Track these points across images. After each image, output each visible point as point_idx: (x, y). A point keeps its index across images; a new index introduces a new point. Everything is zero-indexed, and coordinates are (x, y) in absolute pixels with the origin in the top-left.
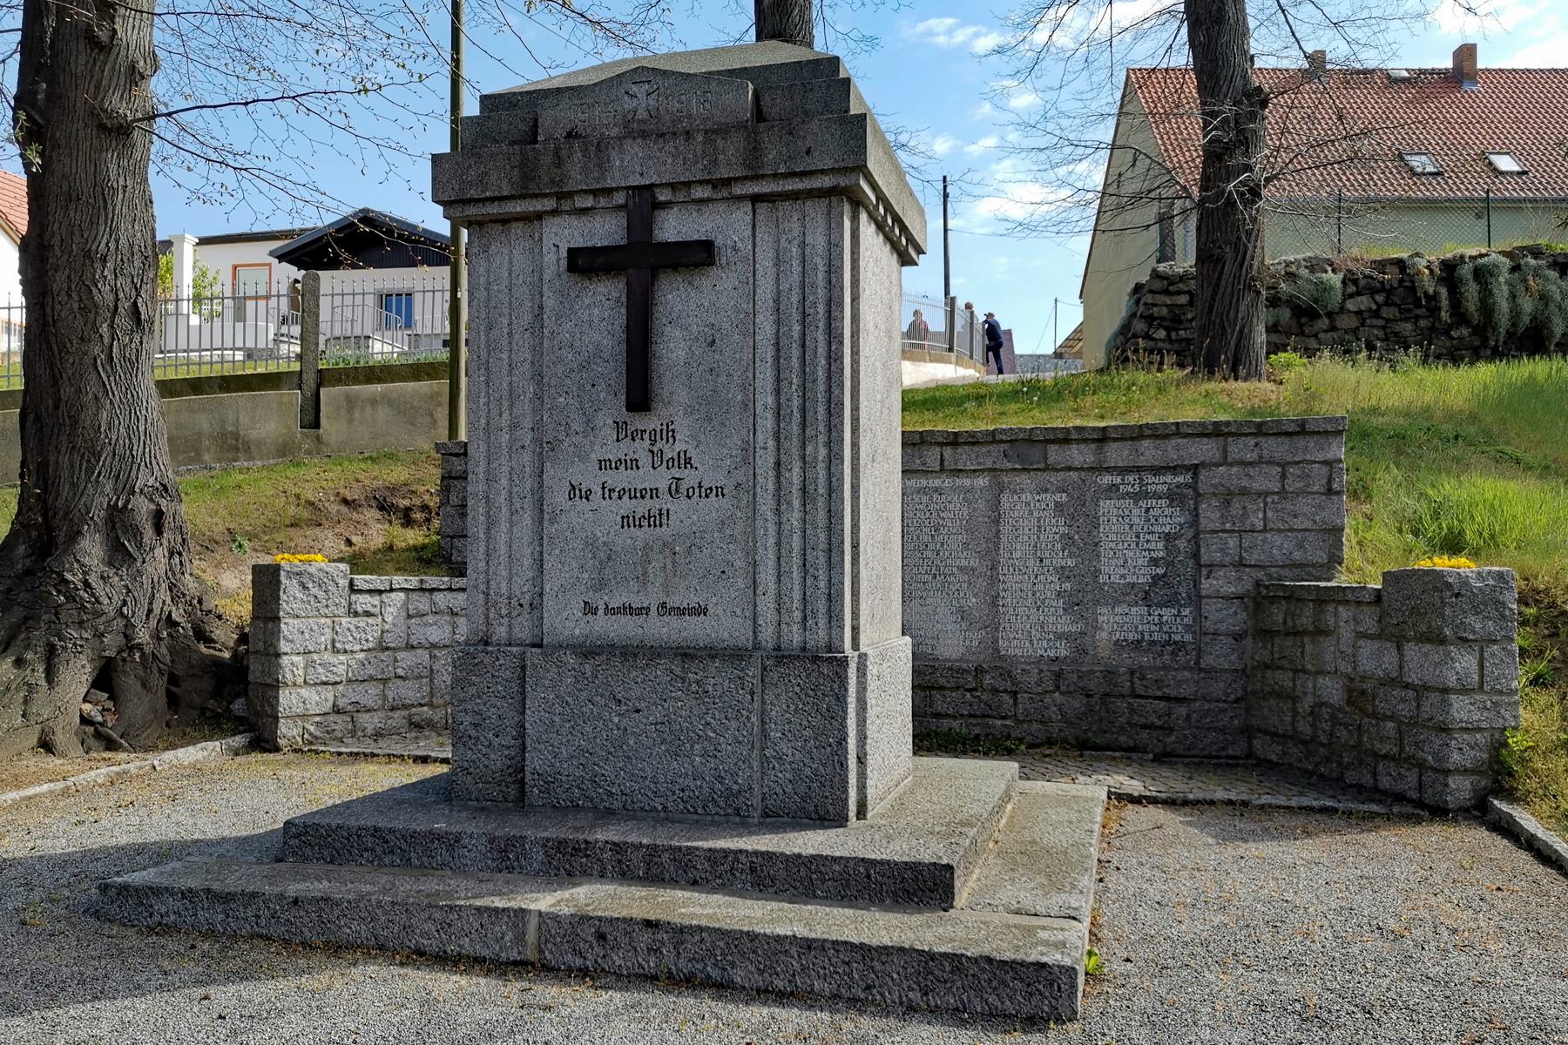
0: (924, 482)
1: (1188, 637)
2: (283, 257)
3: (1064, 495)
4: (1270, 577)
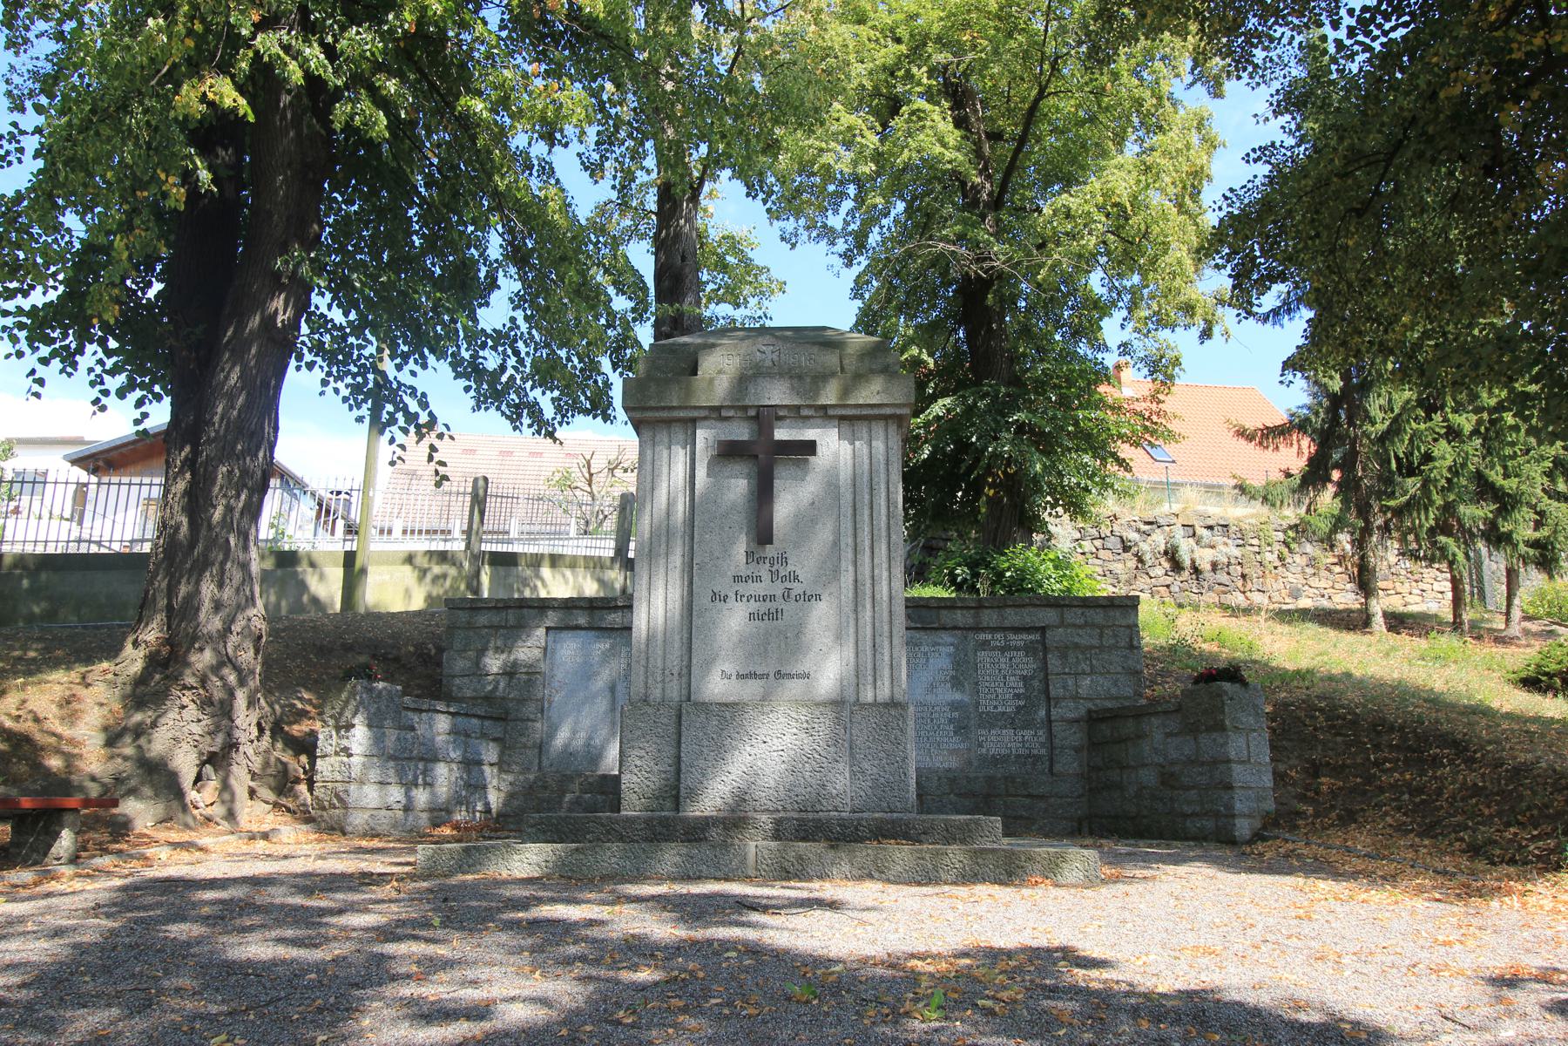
1: (1043, 751)
2: (78, 461)
4: (1096, 705)
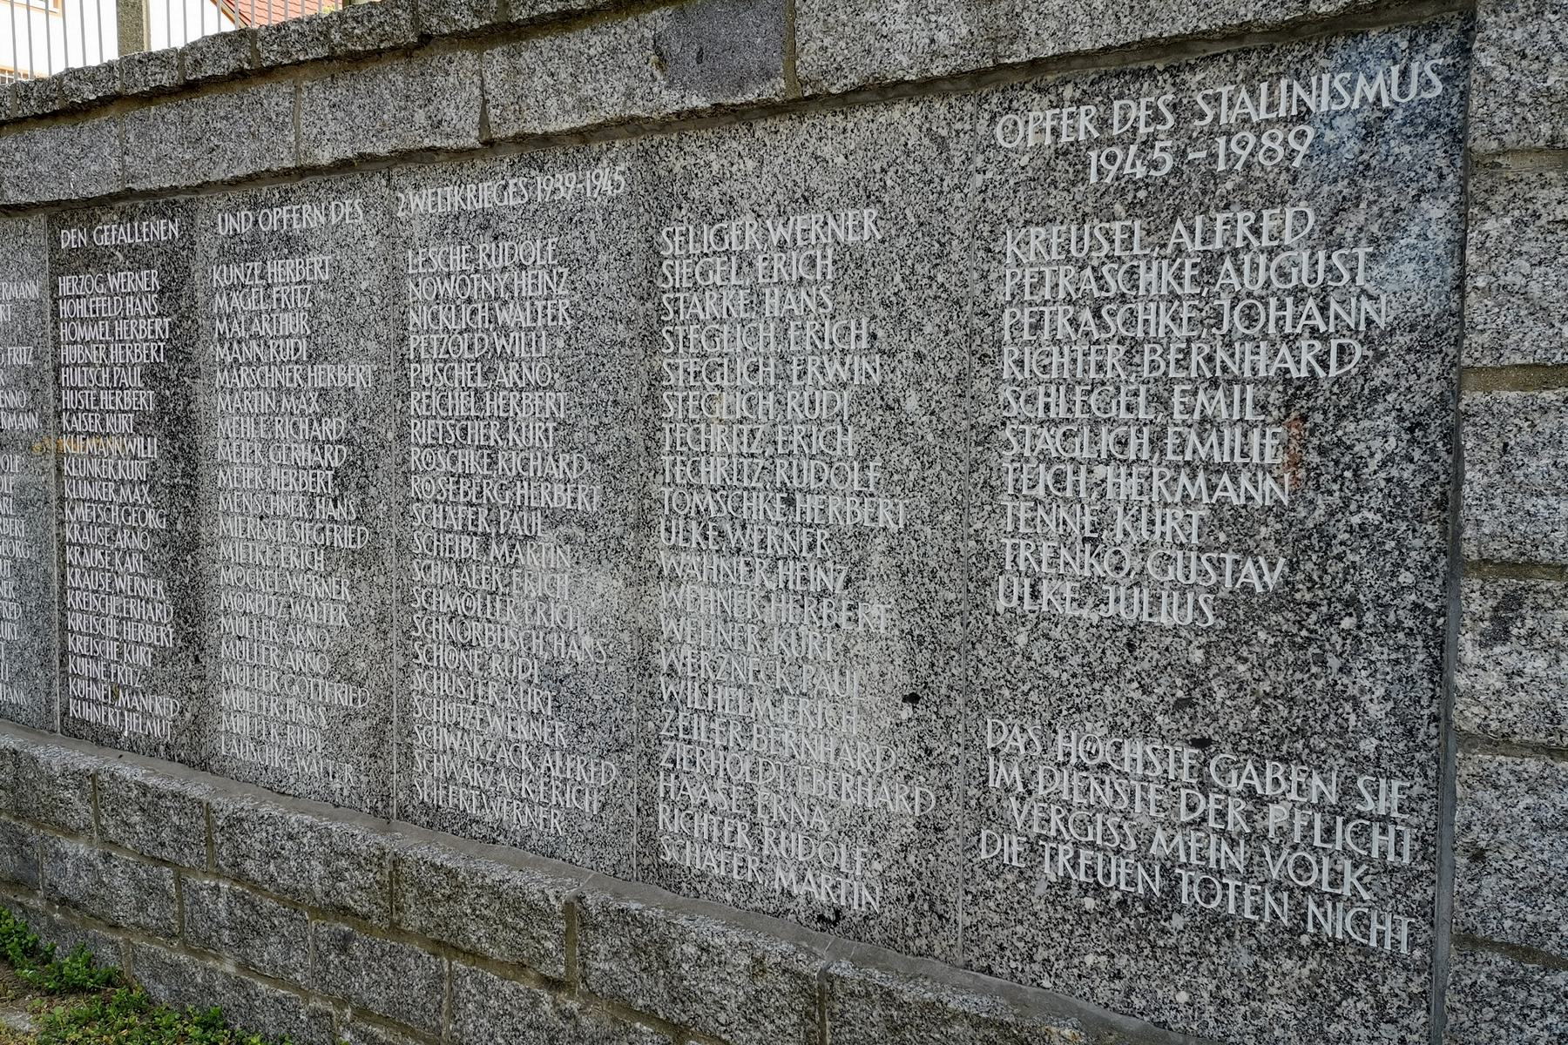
0: (453, 197)
3: (869, 214)
